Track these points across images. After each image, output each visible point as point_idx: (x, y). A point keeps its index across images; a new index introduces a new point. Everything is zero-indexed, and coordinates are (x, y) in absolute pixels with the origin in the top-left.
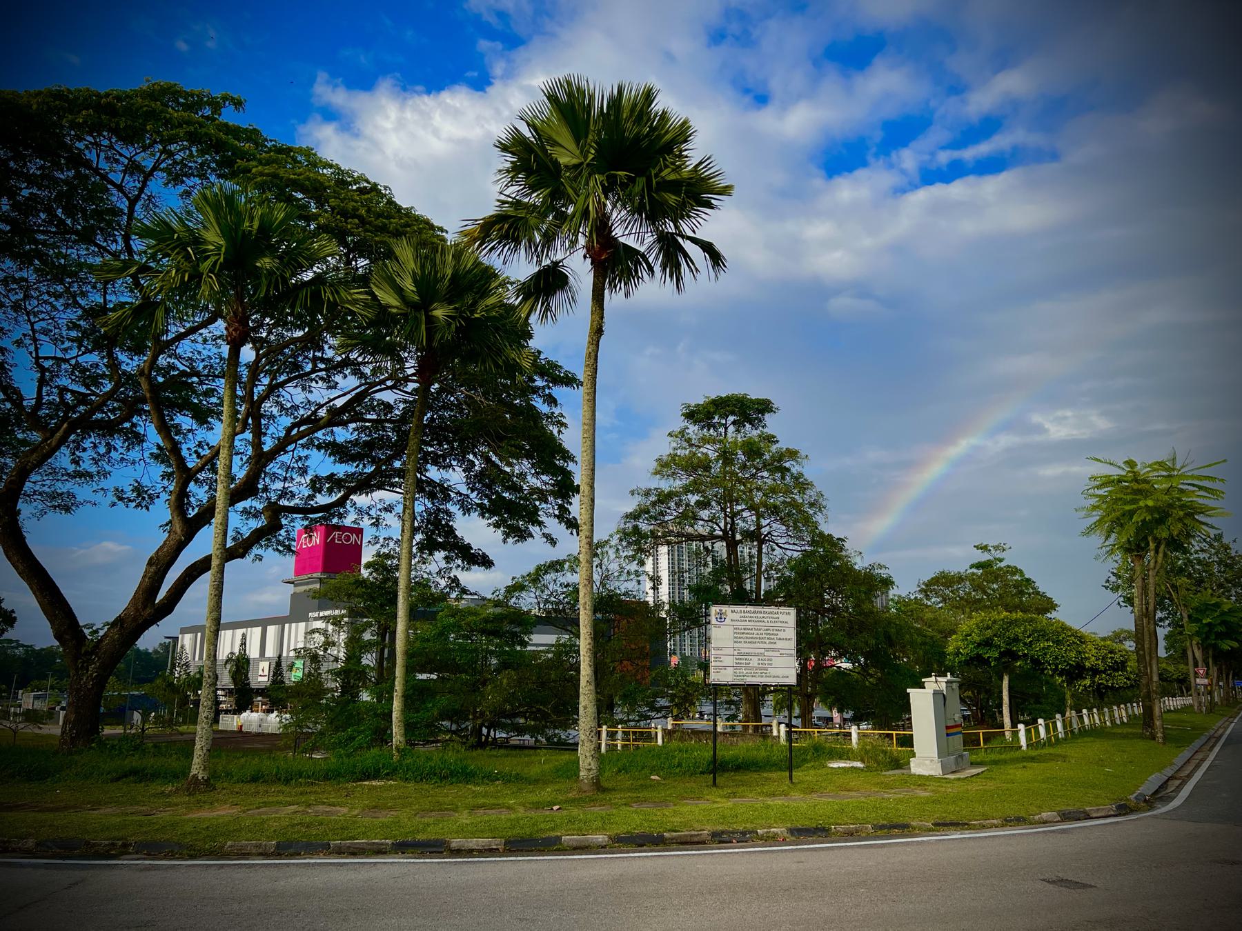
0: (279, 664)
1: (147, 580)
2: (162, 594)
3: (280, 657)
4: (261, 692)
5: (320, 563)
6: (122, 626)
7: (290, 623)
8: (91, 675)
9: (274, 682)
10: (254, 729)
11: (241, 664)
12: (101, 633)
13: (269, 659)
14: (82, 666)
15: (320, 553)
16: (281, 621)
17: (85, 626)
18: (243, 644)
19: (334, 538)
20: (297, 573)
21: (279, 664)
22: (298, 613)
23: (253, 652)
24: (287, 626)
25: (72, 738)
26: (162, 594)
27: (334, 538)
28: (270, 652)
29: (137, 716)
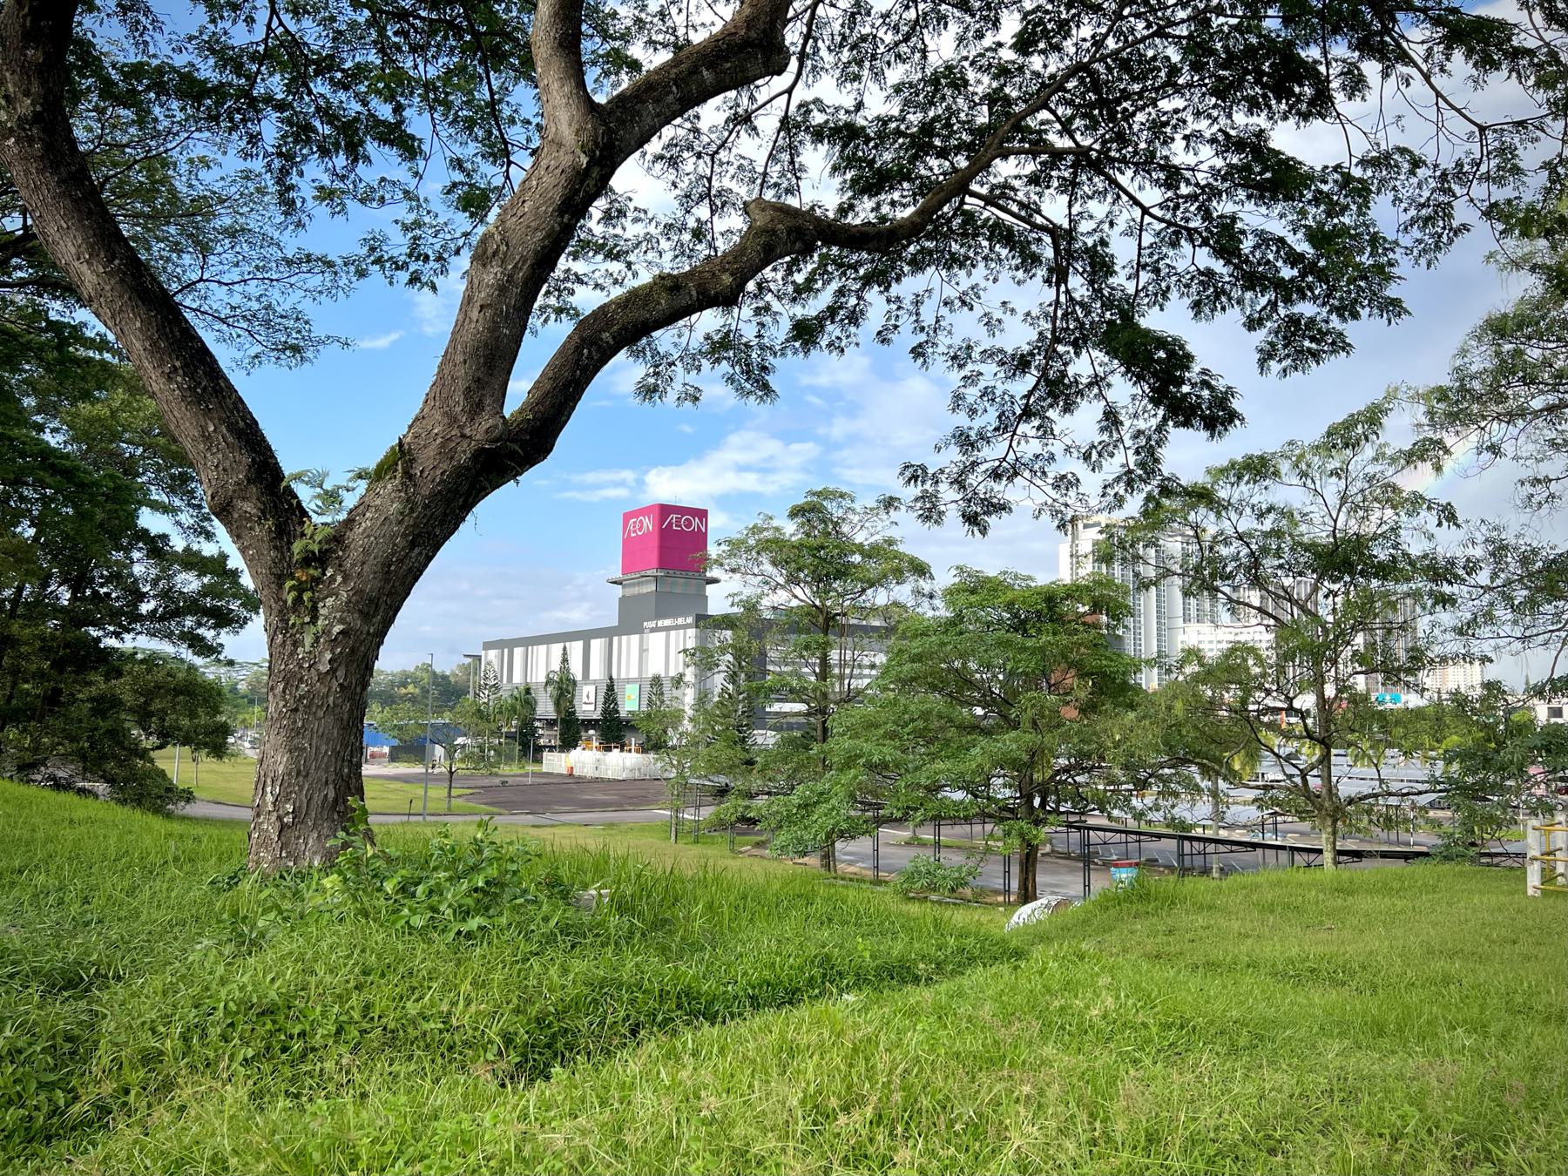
0: (611, 688)
1: (475, 314)
2: (520, 388)
3: (611, 678)
4: (589, 724)
5: (654, 556)
6: (408, 475)
7: (620, 635)
8: (326, 631)
9: (605, 711)
10: (589, 772)
11: (564, 688)
12: (350, 500)
13: (594, 682)
14: (298, 600)
15: (654, 544)
16: (607, 633)
17: (298, 477)
18: (565, 660)
19: (670, 524)
20: (626, 569)
21: (611, 688)
22: (631, 620)
23: (576, 669)
24: (615, 639)
25: (283, 828)
26: (520, 388)
27: (670, 524)
28: (597, 672)
29: (439, 751)
